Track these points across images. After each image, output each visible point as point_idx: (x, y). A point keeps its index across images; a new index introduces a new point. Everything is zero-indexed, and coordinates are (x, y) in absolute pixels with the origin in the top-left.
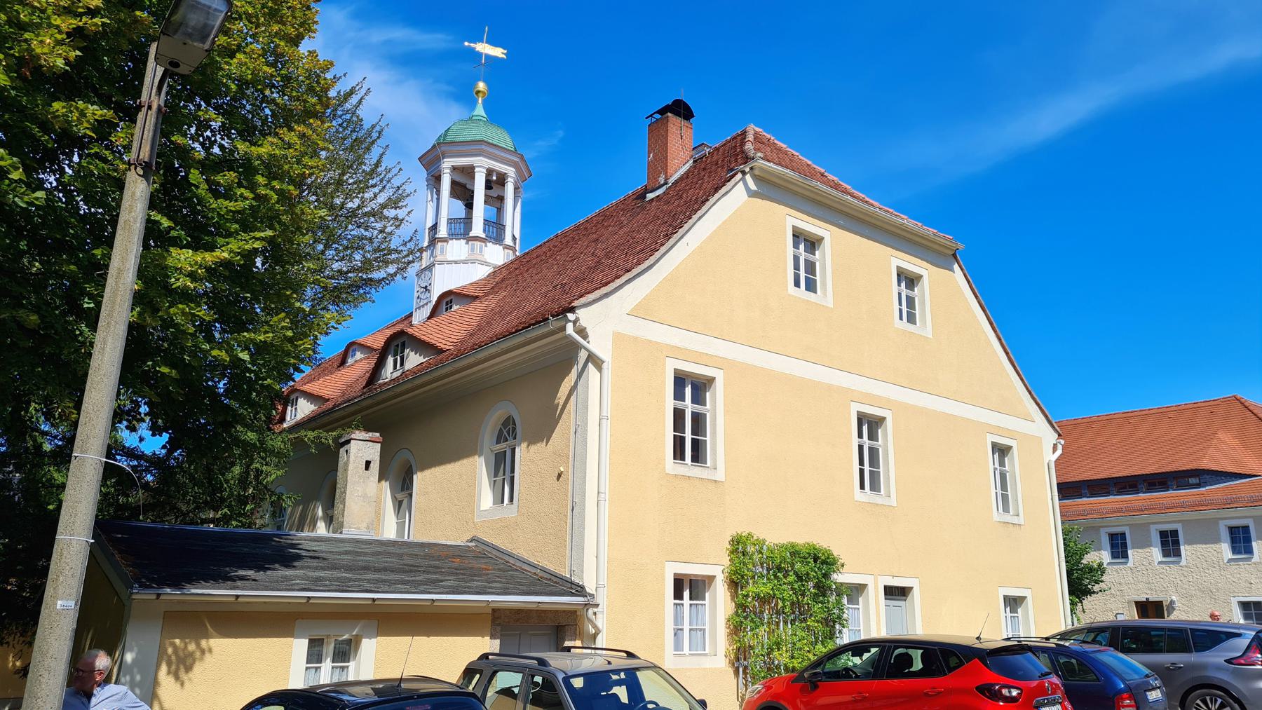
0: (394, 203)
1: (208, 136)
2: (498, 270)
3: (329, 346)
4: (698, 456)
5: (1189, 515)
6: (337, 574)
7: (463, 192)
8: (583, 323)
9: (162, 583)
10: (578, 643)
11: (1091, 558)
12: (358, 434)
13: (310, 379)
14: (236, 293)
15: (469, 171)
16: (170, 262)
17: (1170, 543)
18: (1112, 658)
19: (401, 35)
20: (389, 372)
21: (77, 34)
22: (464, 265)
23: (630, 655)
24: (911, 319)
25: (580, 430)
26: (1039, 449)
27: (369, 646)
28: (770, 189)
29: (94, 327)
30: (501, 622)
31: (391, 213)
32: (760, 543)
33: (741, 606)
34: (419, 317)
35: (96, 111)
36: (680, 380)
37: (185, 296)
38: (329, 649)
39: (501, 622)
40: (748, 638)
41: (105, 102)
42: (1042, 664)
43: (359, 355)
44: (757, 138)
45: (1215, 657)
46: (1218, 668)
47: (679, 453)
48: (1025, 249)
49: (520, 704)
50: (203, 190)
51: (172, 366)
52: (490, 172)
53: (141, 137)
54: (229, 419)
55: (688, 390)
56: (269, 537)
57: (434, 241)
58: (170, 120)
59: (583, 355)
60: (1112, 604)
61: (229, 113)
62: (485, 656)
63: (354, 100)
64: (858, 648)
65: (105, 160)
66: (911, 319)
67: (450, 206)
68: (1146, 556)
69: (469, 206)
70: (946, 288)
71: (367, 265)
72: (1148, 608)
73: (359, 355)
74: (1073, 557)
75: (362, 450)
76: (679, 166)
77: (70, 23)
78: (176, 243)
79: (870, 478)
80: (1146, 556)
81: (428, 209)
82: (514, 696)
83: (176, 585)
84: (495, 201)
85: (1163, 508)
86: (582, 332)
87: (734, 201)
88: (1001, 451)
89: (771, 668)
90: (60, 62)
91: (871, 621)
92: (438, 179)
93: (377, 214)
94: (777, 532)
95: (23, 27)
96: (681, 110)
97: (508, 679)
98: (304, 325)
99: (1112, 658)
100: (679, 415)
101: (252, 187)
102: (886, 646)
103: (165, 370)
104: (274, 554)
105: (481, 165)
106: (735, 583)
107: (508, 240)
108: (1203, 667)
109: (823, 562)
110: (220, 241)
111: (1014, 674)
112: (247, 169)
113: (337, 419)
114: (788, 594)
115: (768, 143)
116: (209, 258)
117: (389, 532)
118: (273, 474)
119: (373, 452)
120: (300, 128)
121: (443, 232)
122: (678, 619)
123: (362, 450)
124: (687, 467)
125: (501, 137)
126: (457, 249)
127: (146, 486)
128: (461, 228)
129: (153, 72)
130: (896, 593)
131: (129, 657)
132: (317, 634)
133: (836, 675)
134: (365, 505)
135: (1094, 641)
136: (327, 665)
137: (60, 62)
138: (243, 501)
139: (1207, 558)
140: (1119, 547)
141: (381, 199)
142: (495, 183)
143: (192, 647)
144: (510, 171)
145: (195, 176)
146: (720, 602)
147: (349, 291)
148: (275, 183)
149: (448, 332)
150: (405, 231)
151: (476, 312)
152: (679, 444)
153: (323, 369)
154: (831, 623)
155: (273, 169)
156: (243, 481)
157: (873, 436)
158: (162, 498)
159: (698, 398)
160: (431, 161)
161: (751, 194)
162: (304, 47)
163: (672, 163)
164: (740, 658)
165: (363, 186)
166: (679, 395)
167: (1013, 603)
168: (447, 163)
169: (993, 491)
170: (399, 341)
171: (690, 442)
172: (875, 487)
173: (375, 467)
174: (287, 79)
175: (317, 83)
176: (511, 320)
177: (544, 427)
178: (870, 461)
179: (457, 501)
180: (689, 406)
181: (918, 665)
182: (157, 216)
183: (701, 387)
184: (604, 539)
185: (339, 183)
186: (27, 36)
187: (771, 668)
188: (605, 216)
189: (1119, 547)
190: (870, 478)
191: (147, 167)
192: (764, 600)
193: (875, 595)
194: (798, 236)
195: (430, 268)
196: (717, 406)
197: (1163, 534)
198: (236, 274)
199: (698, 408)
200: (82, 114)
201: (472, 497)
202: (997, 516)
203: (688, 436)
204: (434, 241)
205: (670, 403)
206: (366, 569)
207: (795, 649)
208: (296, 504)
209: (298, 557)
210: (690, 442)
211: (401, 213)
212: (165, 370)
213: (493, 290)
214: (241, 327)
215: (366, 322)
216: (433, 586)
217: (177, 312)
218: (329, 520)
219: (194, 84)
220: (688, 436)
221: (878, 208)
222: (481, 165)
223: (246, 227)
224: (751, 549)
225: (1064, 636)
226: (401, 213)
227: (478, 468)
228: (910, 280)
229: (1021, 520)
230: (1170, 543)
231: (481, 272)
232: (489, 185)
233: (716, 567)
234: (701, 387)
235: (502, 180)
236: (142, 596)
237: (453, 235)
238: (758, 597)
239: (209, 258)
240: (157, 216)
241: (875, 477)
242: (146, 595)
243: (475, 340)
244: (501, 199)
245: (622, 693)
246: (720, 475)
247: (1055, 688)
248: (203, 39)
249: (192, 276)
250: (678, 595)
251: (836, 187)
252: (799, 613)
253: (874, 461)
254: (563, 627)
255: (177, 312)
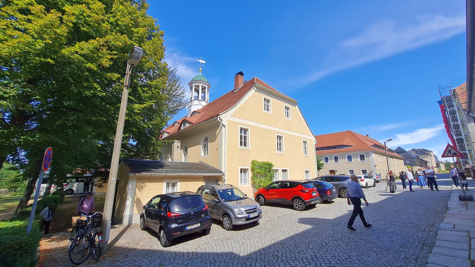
0: (182, 93)
1: (142, 80)
2: (204, 106)
3: (170, 123)
4: (245, 145)
5: (340, 154)
6: (172, 169)
7: (197, 91)
8: (221, 118)
9: (136, 172)
10: (221, 183)
11: (321, 162)
12: (176, 141)
13: (167, 129)
14: (149, 113)
15: (198, 86)
16: (134, 107)
17: (336, 159)
18: (326, 183)
19: (188, 59)
20: (182, 128)
21: (111, 59)
22: (197, 106)
23: (231, 186)
24: (288, 116)
25: (221, 139)
26: (312, 142)
27: (179, 184)
28: (260, 90)
29: (118, 120)
30: (206, 179)
31: (182, 95)
32: (258, 162)
33: (254, 174)
34: (189, 116)
35: (117, 75)
36: (241, 129)
37: (137, 114)
38: (171, 185)
39: (206, 179)
40: (255, 181)
41: (119, 73)
42: (312, 185)
43: (177, 124)
44: (257, 79)
45: (345, 183)
46: (346, 184)
47: (241, 144)
48: (308, 101)
49: (209, 195)
50: (141, 91)
51: (136, 129)
52: (202, 86)
53: (126, 80)
54: (149, 139)
55: (243, 132)
56: (158, 162)
57: (191, 101)
58: (132, 77)
59: (221, 124)
60: (325, 172)
61: (146, 75)
62: (202, 186)
63: (174, 72)
64: (277, 183)
65: (119, 86)
66: (288, 116)
67: (195, 94)
68: (332, 162)
69: (198, 93)
70: (295, 110)
71: (177, 106)
72: (332, 172)
73: (177, 124)
74: (318, 162)
75: (177, 144)
76: (241, 85)
77: (110, 57)
78: (136, 103)
79: (280, 149)
80: (332, 162)
81: (189, 95)
82: (208, 194)
83: (139, 173)
84: (204, 92)
85: (335, 152)
86: (221, 120)
87: (252, 92)
88: (305, 142)
89: (260, 186)
90: (108, 65)
91: (279, 177)
92: (192, 88)
93: (179, 95)
94: (262, 159)
95: (100, 57)
96: (241, 74)
97: (206, 191)
98: (163, 120)
99: (326, 183)
100: (241, 136)
101: (152, 91)
102: (282, 182)
103: (134, 129)
104: (159, 165)
105: (201, 85)
106: (252, 170)
107: (206, 101)
108: (344, 184)
109: (270, 165)
110: (145, 102)
111: (307, 188)
112: (150, 87)
113: (172, 137)
114: (263, 172)
115: (259, 80)
116: (142, 106)
117: (183, 161)
118: (159, 149)
119: (179, 144)
120: (161, 78)
121: (193, 99)
122: (241, 177)
123: (177, 144)
124: (243, 147)
125: (205, 79)
126: (196, 102)
127: (134, 151)
128: (197, 98)
129: (128, 66)
130: (284, 171)
131: (130, 187)
132: (168, 182)
133: (272, 188)
134: (178, 155)
135: (322, 180)
136: (170, 188)
137: (108, 65)
138: (154, 154)
139: (343, 162)
140: (327, 160)
141: (180, 92)
142: (203, 89)
143: (143, 185)
144: (207, 86)
145: (139, 89)
146: (250, 174)
147: (173, 112)
148: (156, 90)
149: (194, 120)
150: (185, 99)
151: (200, 115)
152: (241, 142)
153: (170, 127)
154: (272, 177)
155: (156, 88)
156: (153, 150)
157: (280, 140)
158: (137, 154)
159: (245, 133)
160: (190, 84)
161: (256, 91)
162: (162, 60)
163: (239, 85)
164: (253, 185)
165: (176, 90)
166: (241, 132)
167: (307, 172)
168: (194, 85)
169: (303, 150)
170: (184, 122)
171: (243, 142)
172: (280, 150)
173: (180, 147)
174: (158, 68)
175: (165, 68)
176: (207, 117)
177: (213, 140)
178: (279, 145)
179: (196, 154)
180: (243, 135)
181: (288, 185)
182: (131, 97)
183: (245, 131)
184: (226, 162)
185: (171, 89)
186: (101, 59)
187: (260, 186)
188: (226, 95)
189: (327, 160)
190: (280, 149)
191: (127, 87)
192: (258, 173)
193: (280, 171)
194: (265, 99)
195: (190, 106)
196: (249, 134)
197: (335, 157)
198: (150, 109)
199: (245, 135)
200: (114, 76)
201: (200, 154)
202: (304, 155)
203: (243, 141)
204: (191, 101)
205: (239, 134)
206: (178, 168)
207: (265, 183)
208: (164, 154)
209: (164, 166)
210: (243, 142)
211: (184, 95)
212: (134, 129)
213: (203, 111)
214: (151, 120)
215: (178, 118)
216: (192, 172)
217: (137, 118)
218: (171, 157)
219: (138, 69)
220: (243, 141)
221: (281, 94)
222: (201, 85)
223: (150, 99)
224: (256, 163)
225: (316, 179)
226: (184, 95)
227: (200, 147)
228: (287, 108)
229: (308, 156)
230: (336, 159)
231: (201, 107)
232: (202, 89)
233: (249, 167)
234: (245, 131)
235: (205, 88)
236: (131, 175)
237: (195, 100)
238: (257, 173)
239: (142, 106)
240: (131, 97)
241: (280, 148)
242: (133, 174)
243: (199, 121)
244: (205, 92)
245: (230, 193)
246: (249, 148)
247: (315, 190)
248: (138, 59)
249: (139, 110)
250: (241, 172)
251: (273, 89)
252: (266, 176)
253: (280, 145)
254: (218, 179)
255: (137, 118)
